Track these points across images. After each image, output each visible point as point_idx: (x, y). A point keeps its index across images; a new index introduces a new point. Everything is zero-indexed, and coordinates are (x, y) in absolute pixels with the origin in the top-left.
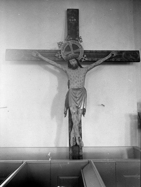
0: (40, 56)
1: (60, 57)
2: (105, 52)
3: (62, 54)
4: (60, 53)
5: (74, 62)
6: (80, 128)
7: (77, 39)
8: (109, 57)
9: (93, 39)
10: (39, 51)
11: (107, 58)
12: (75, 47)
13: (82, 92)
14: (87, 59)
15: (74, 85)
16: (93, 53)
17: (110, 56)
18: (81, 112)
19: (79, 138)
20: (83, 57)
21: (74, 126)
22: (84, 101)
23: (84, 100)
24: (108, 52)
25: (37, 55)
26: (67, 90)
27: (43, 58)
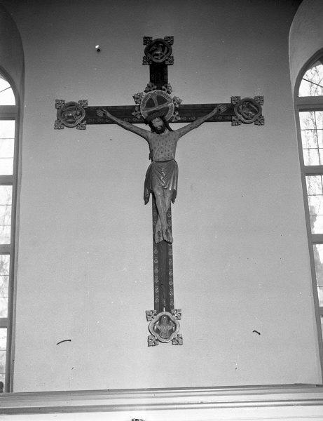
0: (108, 115)
1: (139, 117)
2: (158, 300)
3: (142, 112)
4: (139, 110)
5: (158, 123)
6: (169, 219)
7: (164, 87)
8: (213, 114)
9: (185, 88)
10: (107, 108)
11: (209, 116)
12: (162, 100)
13: (171, 166)
14: (179, 119)
15: (160, 156)
16: (168, 251)
17: (215, 111)
18: (169, 195)
19: (167, 230)
20: (173, 115)
21: (159, 76)
22: (174, 178)
23: (173, 182)
24: (213, 107)
25: (104, 114)
26: (150, 162)
27: (114, 118)
